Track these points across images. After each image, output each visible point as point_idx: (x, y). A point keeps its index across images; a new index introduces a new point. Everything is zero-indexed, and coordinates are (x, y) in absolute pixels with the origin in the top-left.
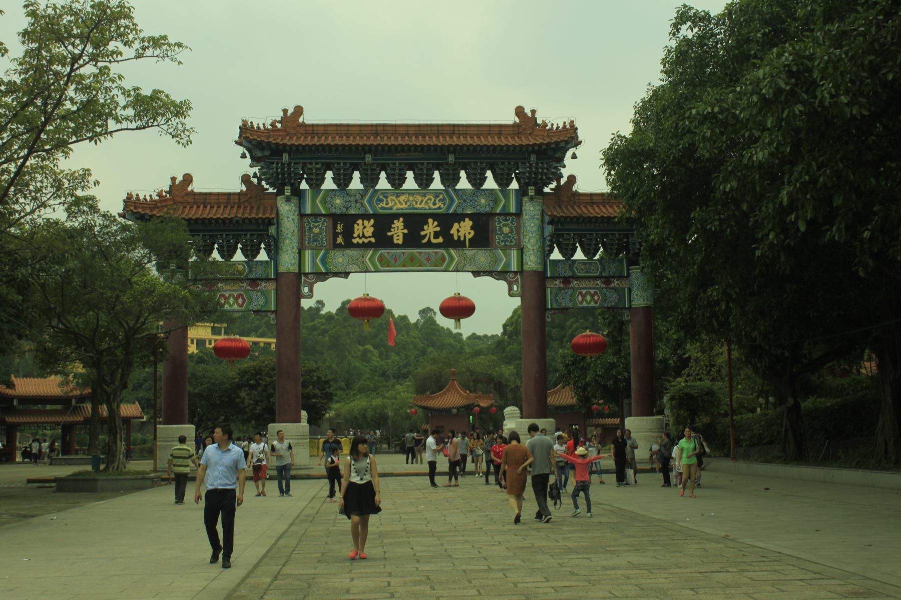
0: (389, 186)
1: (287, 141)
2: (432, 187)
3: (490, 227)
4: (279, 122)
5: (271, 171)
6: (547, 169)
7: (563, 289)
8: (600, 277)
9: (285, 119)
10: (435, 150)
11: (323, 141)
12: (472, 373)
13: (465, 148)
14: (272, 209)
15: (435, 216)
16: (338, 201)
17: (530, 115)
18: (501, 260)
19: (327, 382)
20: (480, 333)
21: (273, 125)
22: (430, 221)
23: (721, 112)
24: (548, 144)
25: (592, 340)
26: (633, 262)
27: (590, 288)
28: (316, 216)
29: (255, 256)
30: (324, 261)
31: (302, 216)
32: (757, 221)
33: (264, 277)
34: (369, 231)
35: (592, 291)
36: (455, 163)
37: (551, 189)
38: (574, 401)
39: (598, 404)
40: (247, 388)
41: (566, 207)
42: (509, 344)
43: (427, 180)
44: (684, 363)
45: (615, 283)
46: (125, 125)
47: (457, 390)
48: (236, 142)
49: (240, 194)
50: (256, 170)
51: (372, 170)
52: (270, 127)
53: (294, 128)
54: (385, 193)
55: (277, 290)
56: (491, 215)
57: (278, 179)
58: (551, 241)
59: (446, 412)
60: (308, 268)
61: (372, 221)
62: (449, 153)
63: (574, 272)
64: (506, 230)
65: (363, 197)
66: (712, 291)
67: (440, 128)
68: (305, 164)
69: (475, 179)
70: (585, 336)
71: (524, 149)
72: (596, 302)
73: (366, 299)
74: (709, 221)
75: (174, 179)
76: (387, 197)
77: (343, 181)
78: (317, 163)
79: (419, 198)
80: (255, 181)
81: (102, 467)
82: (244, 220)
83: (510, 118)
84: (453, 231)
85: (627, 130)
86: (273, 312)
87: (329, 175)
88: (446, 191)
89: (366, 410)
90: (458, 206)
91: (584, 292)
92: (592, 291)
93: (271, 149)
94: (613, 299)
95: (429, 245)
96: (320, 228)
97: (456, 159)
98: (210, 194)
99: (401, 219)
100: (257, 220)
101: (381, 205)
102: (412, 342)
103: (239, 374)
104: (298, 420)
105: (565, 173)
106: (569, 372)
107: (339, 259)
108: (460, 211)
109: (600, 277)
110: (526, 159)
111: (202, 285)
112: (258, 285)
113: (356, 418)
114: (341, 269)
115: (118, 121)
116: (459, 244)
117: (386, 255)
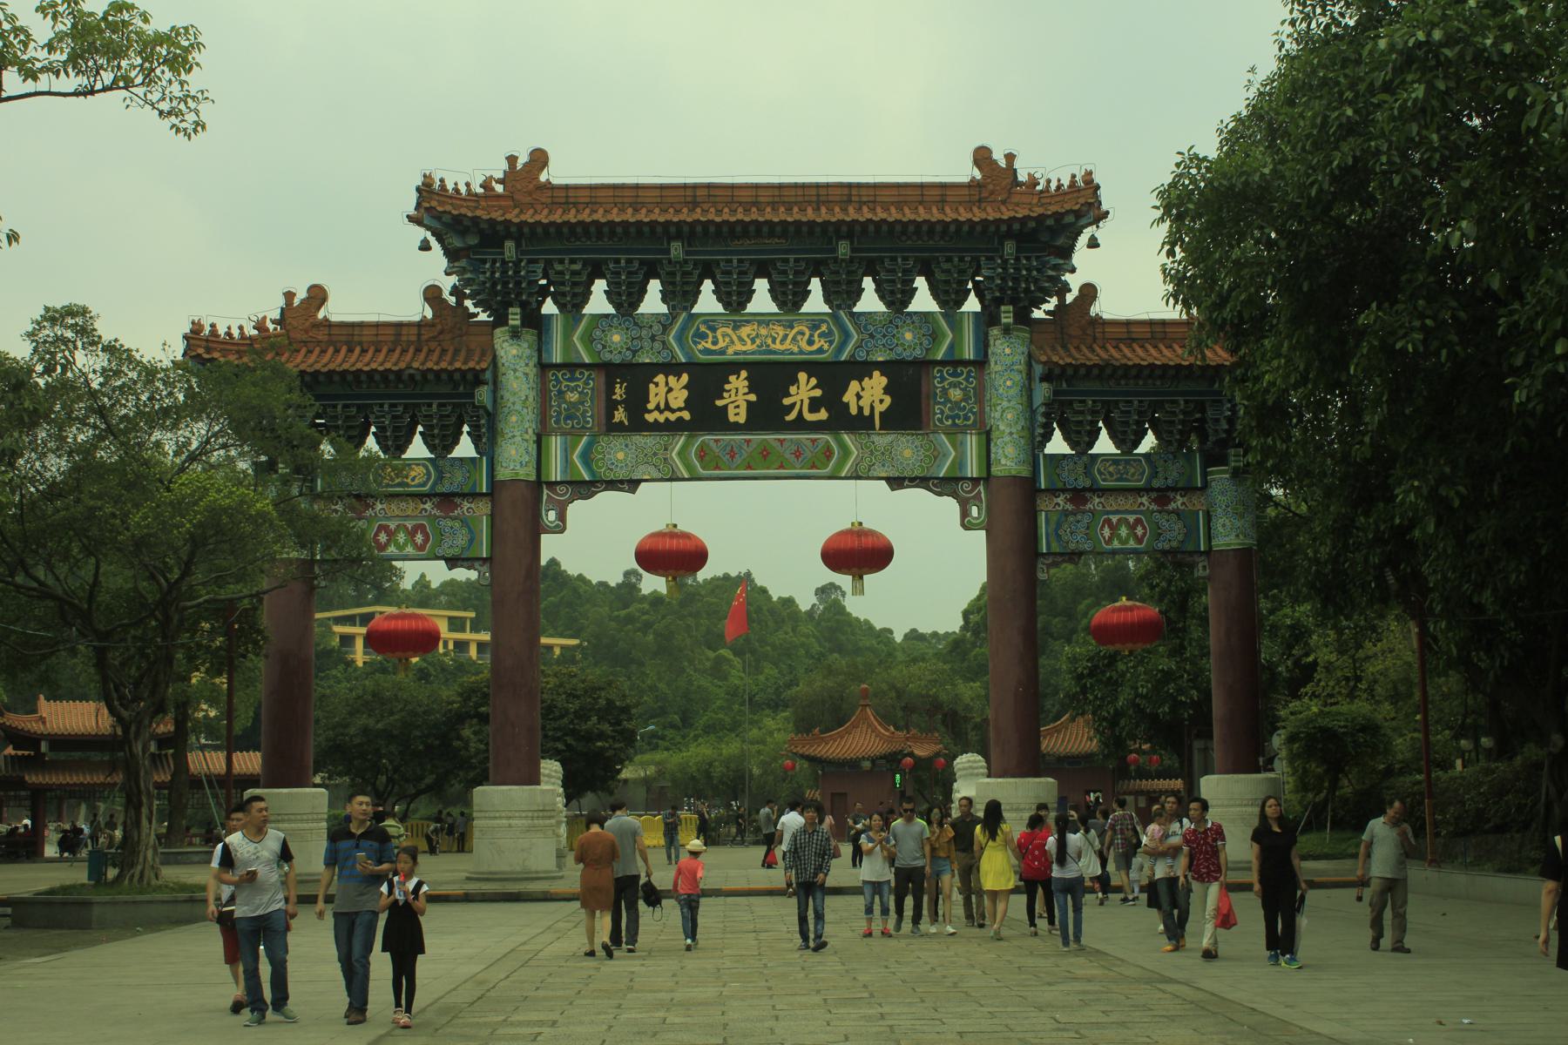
0: (719, 308)
1: (513, 216)
2: (806, 308)
3: (924, 389)
4: (498, 181)
5: (482, 278)
6: (1039, 271)
8: (1147, 490)
9: (513, 174)
10: (811, 233)
11: (585, 216)
12: (900, 694)
13: (871, 228)
14: (483, 354)
15: (812, 367)
16: (616, 338)
18: (946, 455)
19: (625, 710)
20: (925, 629)
21: (486, 185)
22: (802, 376)
23: (1449, 41)
24: (1041, 219)
25: (1134, 616)
26: (1214, 458)
28: (571, 367)
29: (450, 448)
30: (586, 457)
31: (544, 367)
32: (1516, 324)
33: (466, 490)
34: (679, 397)
35: (1131, 518)
36: (852, 260)
37: (1047, 313)
38: (1092, 745)
39: (1140, 750)
40: (475, 721)
41: (1078, 348)
42: (974, 645)
43: (795, 294)
44: (1306, 673)
45: (1178, 502)
46: (44, 82)
47: (870, 725)
49: (422, 325)
50: (454, 279)
51: (685, 274)
52: (480, 191)
53: (530, 194)
54: (711, 321)
55: (492, 516)
56: (925, 364)
57: (496, 294)
58: (1046, 415)
59: (849, 767)
60: (555, 472)
61: (685, 378)
62: (840, 238)
63: (1094, 480)
64: (956, 394)
65: (666, 328)
66: (1407, 492)
67: (823, 192)
68: (549, 263)
69: (892, 292)
70: (1114, 610)
71: (992, 228)
72: (1140, 541)
73: (673, 534)
74: (1401, 332)
75: (289, 296)
76: (714, 330)
77: (626, 298)
78: (573, 261)
79: (781, 331)
81: (112, 873)
82: (424, 373)
83: (963, 171)
84: (849, 397)
85: (1210, 149)
86: (484, 560)
87: (600, 286)
88: (834, 316)
89: (710, 764)
90: (858, 346)
91: (1114, 519)
92: (1131, 518)
93: (481, 233)
94: (1174, 533)
95: (800, 425)
96: (579, 393)
97: (853, 250)
98: (361, 325)
99: (744, 374)
100: (450, 373)
101: (704, 345)
102: (803, 645)
103: (460, 695)
104: (533, 779)
105: (1075, 281)
106: (1084, 690)
107: (619, 453)
108: (861, 356)
109: (1147, 490)
110: (996, 250)
112: (456, 506)
113: (693, 778)
114: (621, 474)
115: (30, 74)
116: (861, 423)
117: (712, 444)
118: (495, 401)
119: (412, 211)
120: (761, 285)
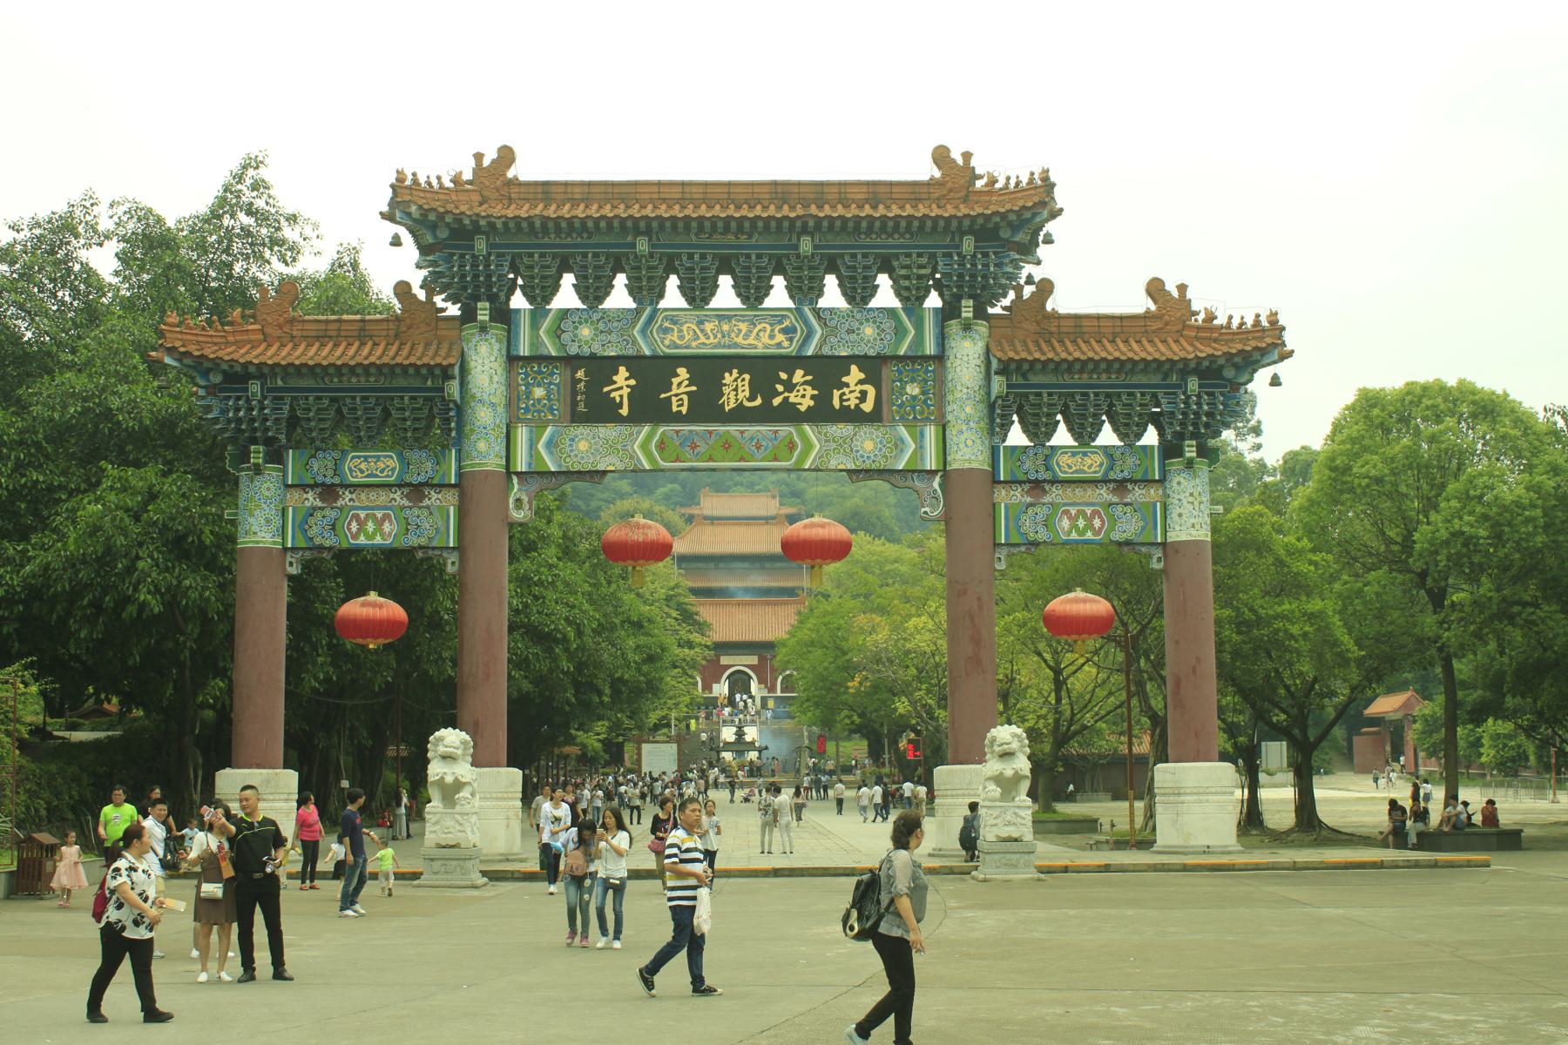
2: (715, 303)
7: (1031, 505)
15: (862, 361)
17: (960, 161)
27: (1088, 504)
31: (512, 359)
33: (1138, 476)
35: (379, 514)
37: (1004, 308)
43: (757, 288)
48: (383, 216)
54: (674, 316)
60: (521, 465)
63: (1054, 473)
67: (687, 189)
77: (593, 291)
78: (920, 255)
79: (743, 327)
80: (421, 295)
83: (925, 171)
91: (362, 514)
92: (379, 514)
97: (815, 247)
108: (826, 351)
109: (1105, 481)
111: (403, 496)
112: (1045, 492)
118: (462, 398)
119: (385, 209)
120: (725, 281)
